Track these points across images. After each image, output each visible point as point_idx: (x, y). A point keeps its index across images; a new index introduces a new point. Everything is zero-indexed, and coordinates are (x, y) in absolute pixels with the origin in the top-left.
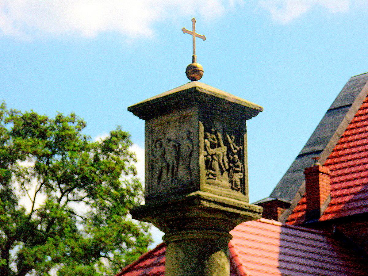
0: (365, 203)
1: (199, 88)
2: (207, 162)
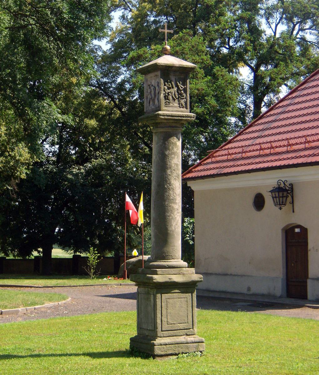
0: (316, 96)
1: (158, 63)
2: (165, 97)
